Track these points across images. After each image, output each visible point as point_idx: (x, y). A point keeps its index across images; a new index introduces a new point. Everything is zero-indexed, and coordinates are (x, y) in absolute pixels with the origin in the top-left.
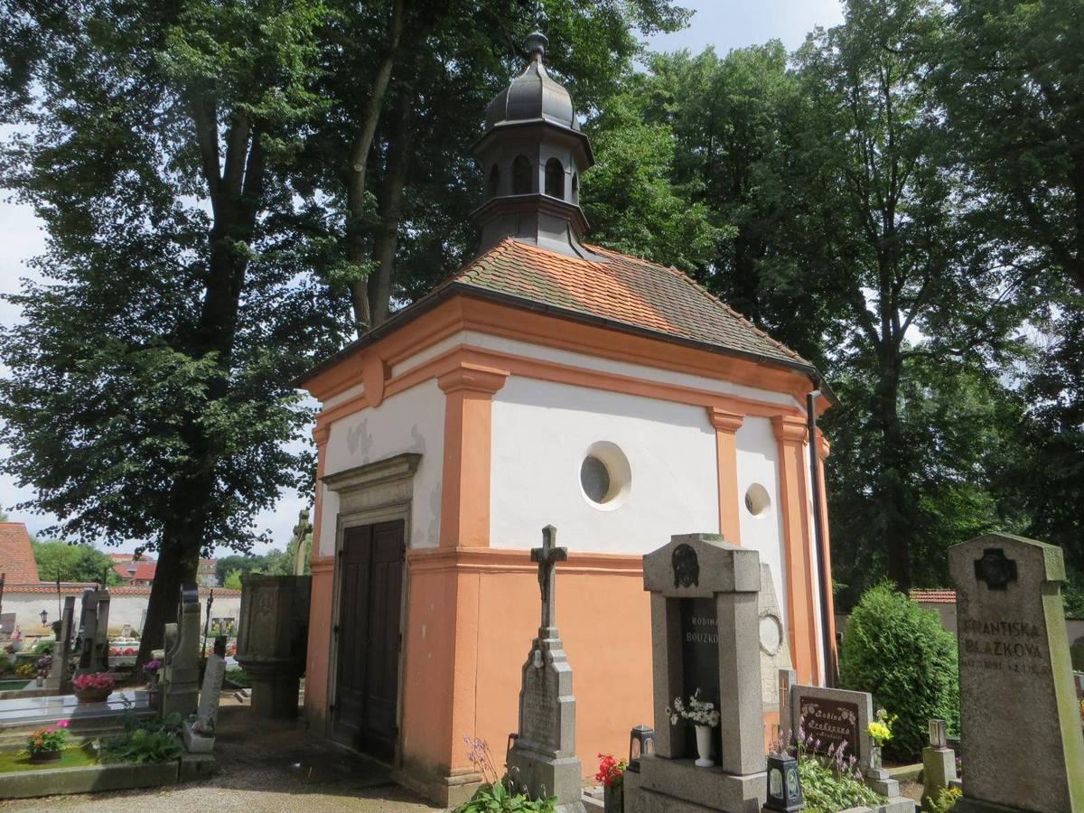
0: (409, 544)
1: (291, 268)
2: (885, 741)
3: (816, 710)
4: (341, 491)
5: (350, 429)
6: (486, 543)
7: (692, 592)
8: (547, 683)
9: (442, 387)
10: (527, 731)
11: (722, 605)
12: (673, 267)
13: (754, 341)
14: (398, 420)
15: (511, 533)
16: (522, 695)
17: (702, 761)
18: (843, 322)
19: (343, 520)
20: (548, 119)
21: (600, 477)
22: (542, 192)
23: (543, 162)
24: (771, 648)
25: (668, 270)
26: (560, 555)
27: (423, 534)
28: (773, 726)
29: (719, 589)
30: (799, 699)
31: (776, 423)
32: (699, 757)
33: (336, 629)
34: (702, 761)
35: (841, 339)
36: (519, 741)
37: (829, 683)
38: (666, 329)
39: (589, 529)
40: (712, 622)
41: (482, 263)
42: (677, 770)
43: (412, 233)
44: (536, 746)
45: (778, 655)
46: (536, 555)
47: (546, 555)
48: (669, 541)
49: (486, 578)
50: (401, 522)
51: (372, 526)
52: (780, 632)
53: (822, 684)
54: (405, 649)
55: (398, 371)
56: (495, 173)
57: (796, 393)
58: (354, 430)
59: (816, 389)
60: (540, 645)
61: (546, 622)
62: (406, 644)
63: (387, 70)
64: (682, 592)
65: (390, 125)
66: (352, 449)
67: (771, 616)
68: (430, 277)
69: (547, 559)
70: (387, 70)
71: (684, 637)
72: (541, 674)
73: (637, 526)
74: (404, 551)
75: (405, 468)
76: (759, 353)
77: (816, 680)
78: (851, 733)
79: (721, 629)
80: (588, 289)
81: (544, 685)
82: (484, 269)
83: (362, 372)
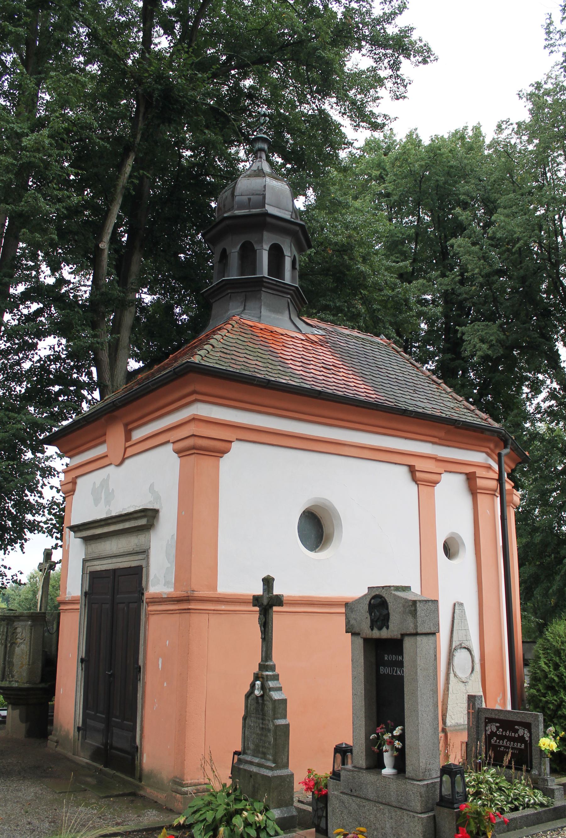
0: (147, 588)
1: (41, 334)
2: (552, 753)
3: (498, 728)
4: (86, 540)
5: (94, 483)
6: (215, 588)
7: (384, 634)
8: (266, 708)
9: (177, 452)
10: (248, 749)
11: (408, 643)
12: (382, 336)
13: (452, 405)
14: (138, 476)
15: (238, 579)
16: (245, 718)
17: (388, 771)
18: (541, 377)
19: (88, 564)
20: (270, 210)
21: (316, 527)
22: (265, 273)
23: (266, 247)
24: (463, 675)
25: (377, 340)
26: (278, 601)
27: (160, 580)
28: (462, 743)
29: (404, 632)
30: (483, 720)
31: (471, 478)
32: (384, 767)
33: (82, 660)
34: (388, 771)
35: (539, 392)
36: (241, 757)
37: (513, 707)
38: (373, 397)
39: (303, 575)
40: (400, 658)
41: (212, 341)
42: (369, 778)
43: (147, 299)
44: (256, 760)
45: (470, 682)
46: (256, 600)
47: (265, 602)
48: (366, 591)
49: (214, 619)
50: (140, 568)
51: (114, 571)
52: (473, 661)
53: (509, 708)
54: (144, 679)
55: (138, 435)
56: (224, 256)
57: (488, 450)
58: (98, 484)
59: (505, 447)
60: (265, 671)
61: (267, 654)
62: (144, 674)
63: (130, 162)
64: (376, 634)
65: (132, 204)
66: (97, 501)
67: (465, 648)
68: (164, 338)
69: (267, 604)
70: (130, 162)
71: (378, 671)
72: (260, 701)
73: (344, 574)
74: (143, 594)
75: (143, 522)
76: (455, 416)
77: (504, 704)
78: (526, 746)
79: (405, 664)
80: (305, 364)
81: (263, 710)
82: (213, 347)
83: (105, 434)
